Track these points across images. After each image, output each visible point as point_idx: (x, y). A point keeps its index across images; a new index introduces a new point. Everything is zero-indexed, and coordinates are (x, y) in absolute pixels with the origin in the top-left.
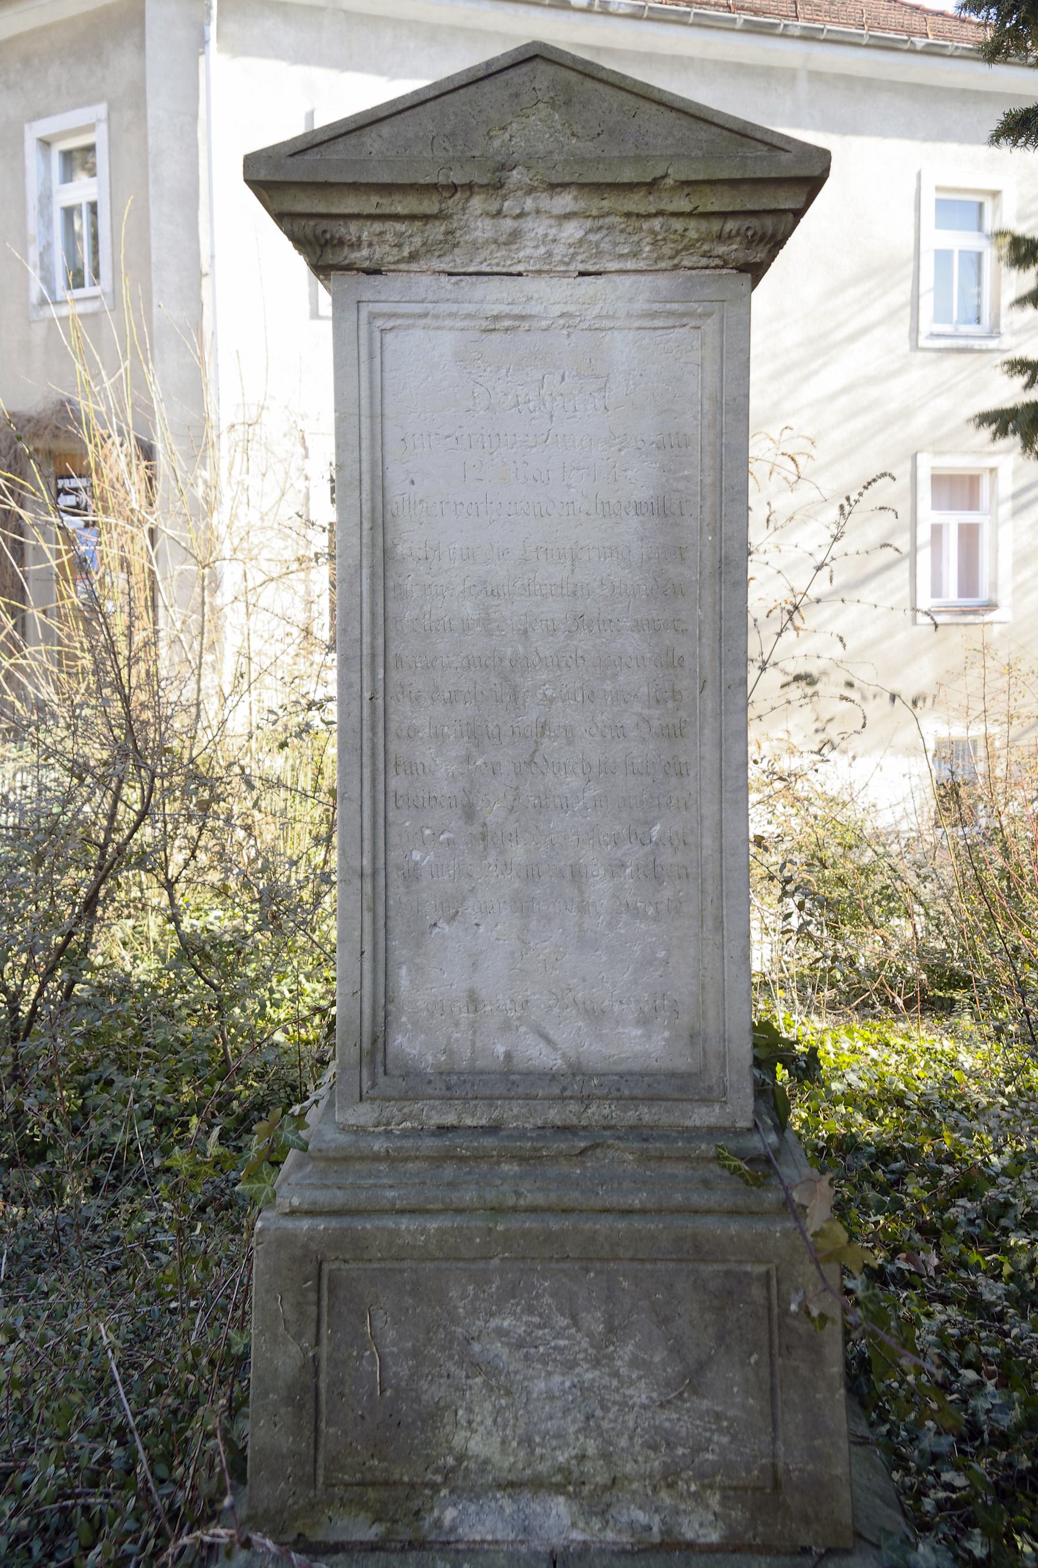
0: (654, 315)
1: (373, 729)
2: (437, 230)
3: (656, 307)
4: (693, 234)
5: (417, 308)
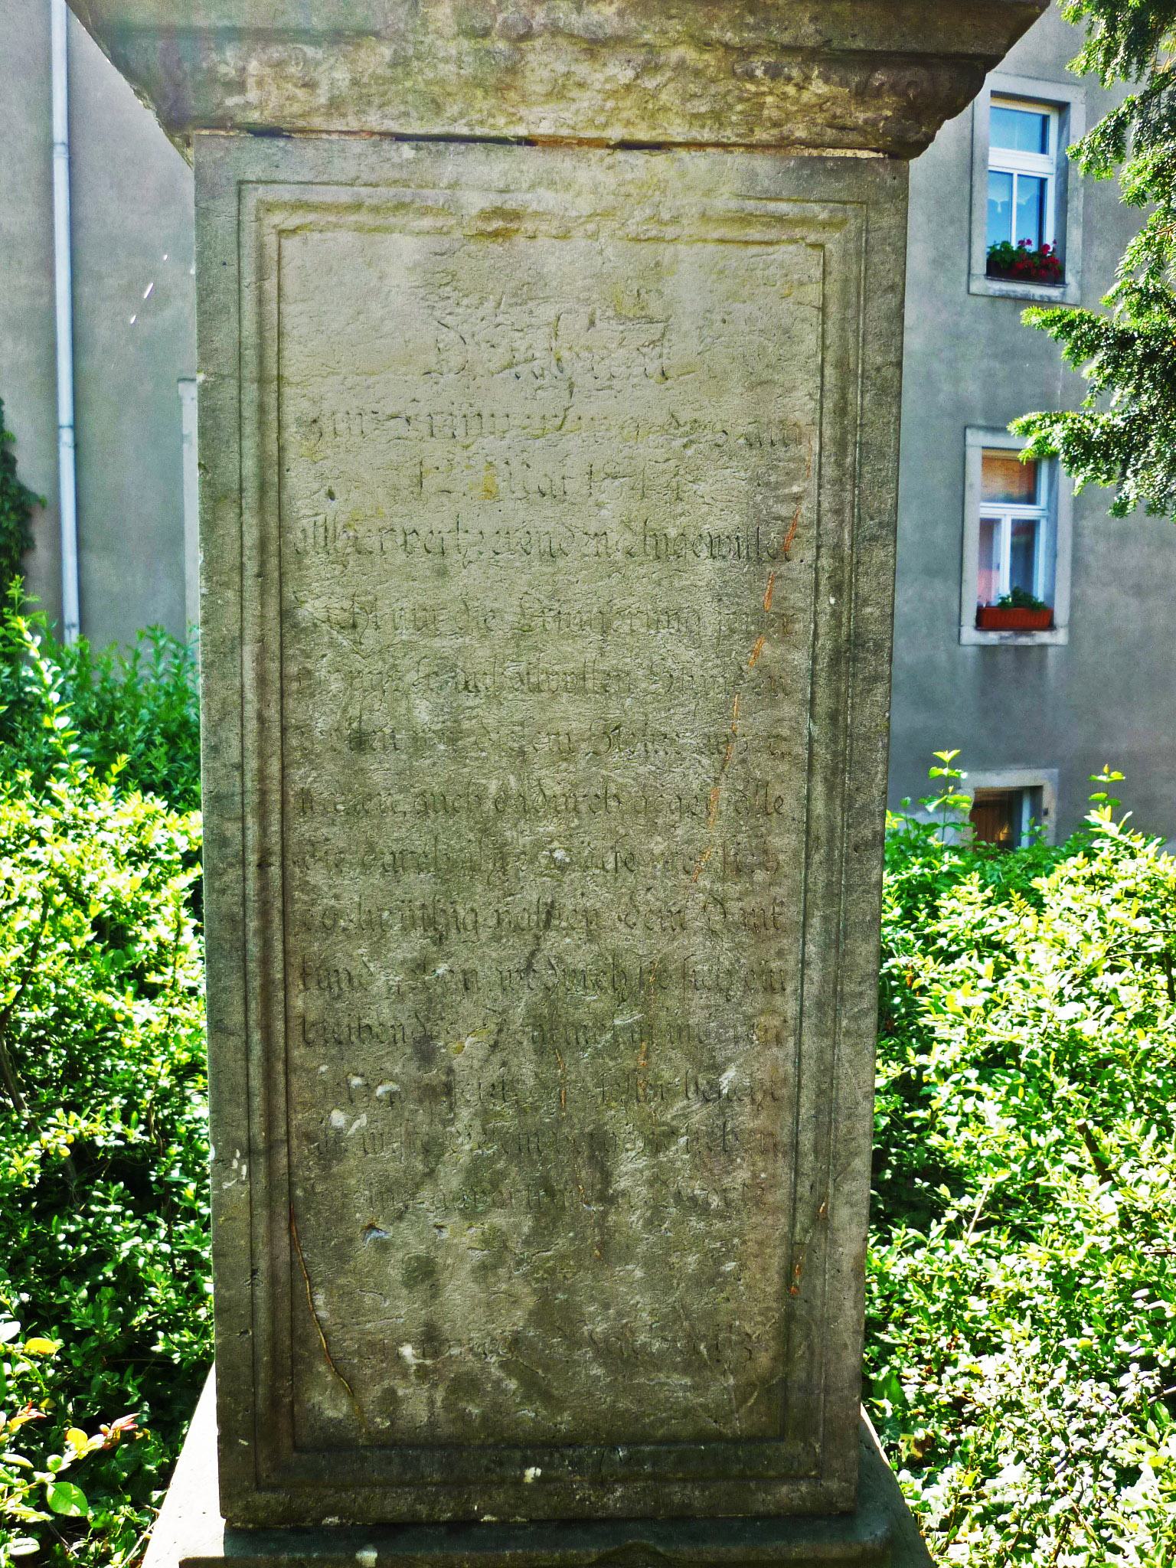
0: (745, 219)
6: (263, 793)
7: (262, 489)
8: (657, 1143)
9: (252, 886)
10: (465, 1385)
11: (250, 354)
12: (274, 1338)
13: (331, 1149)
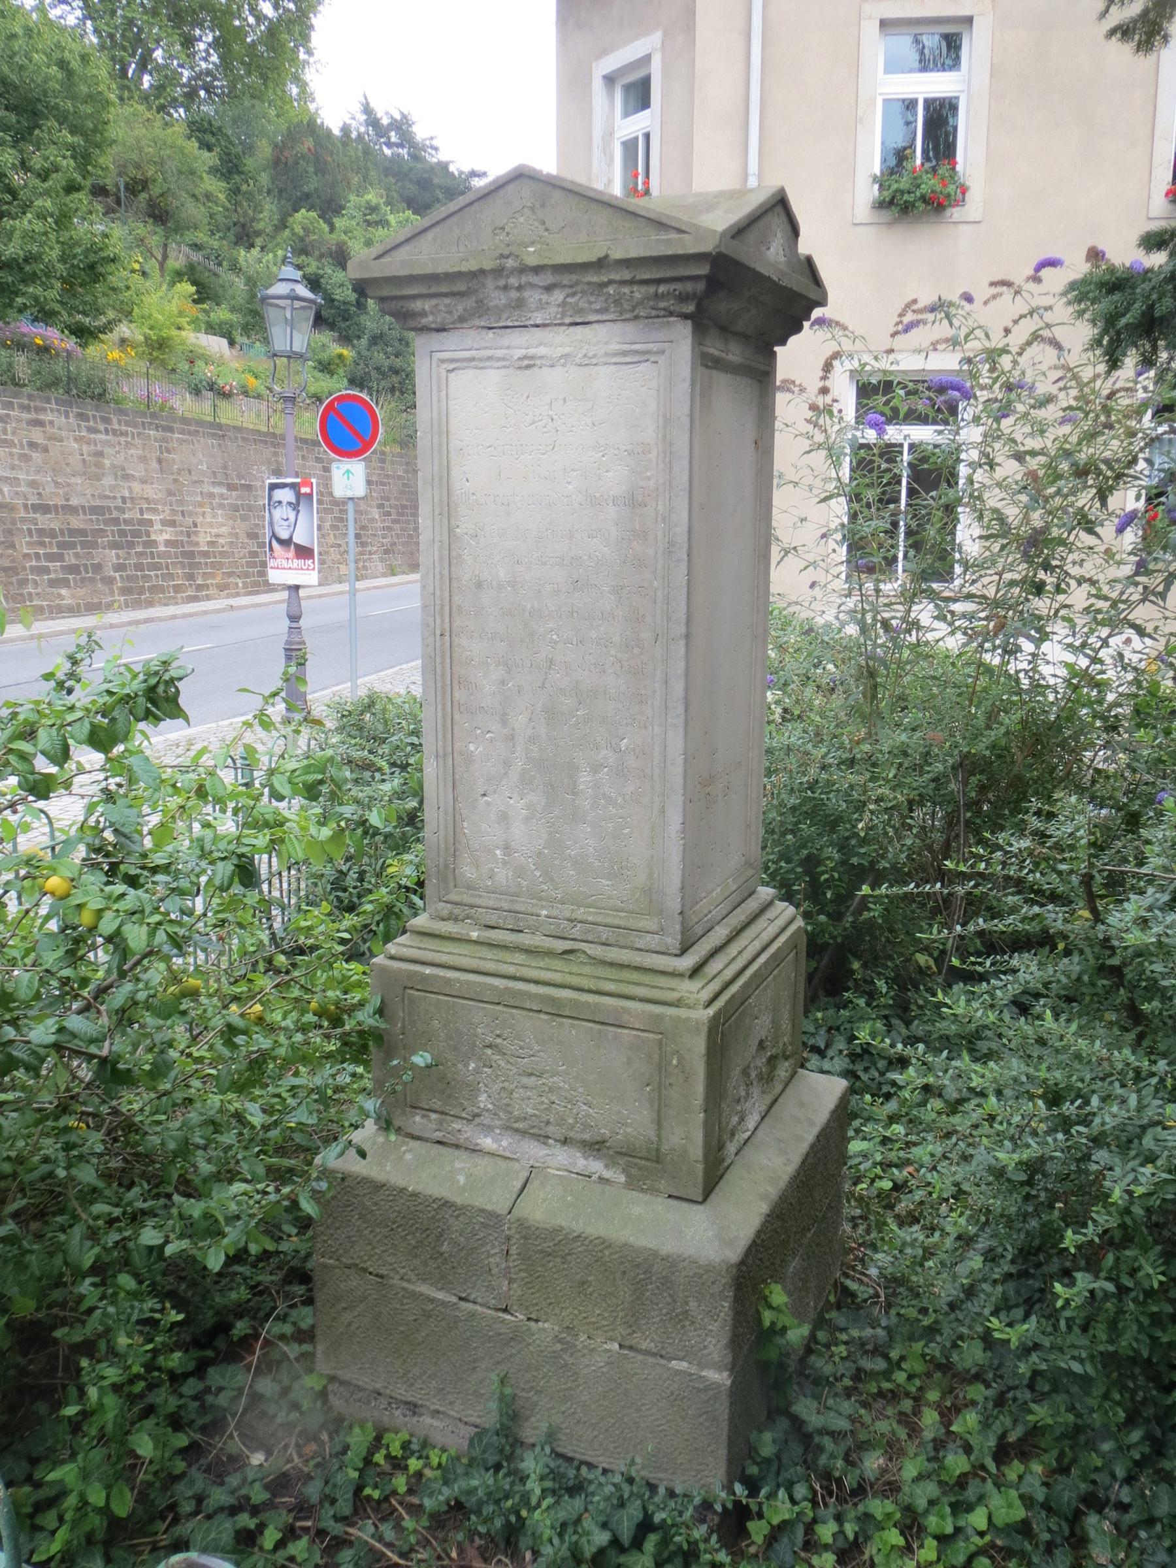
0: (624, 353)
1: (443, 656)
2: (470, 303)
3: (626, 347)
4: (637, 295)
5: (467, 354)
6: (442, 606)
7: (441, 479)
8: (595, 770)
9: (438, 644)
10: (520, 872)
11: (435, 423)
12: (446, 836)
13: (469, 759)
